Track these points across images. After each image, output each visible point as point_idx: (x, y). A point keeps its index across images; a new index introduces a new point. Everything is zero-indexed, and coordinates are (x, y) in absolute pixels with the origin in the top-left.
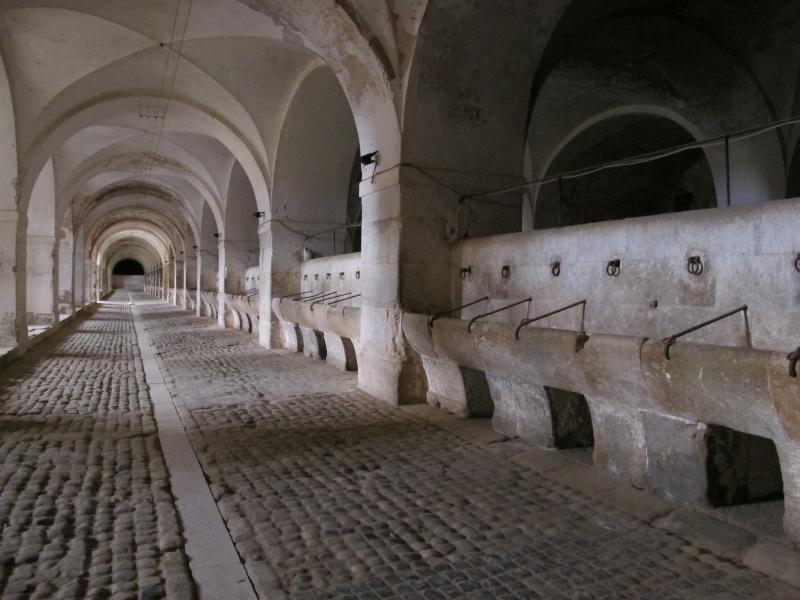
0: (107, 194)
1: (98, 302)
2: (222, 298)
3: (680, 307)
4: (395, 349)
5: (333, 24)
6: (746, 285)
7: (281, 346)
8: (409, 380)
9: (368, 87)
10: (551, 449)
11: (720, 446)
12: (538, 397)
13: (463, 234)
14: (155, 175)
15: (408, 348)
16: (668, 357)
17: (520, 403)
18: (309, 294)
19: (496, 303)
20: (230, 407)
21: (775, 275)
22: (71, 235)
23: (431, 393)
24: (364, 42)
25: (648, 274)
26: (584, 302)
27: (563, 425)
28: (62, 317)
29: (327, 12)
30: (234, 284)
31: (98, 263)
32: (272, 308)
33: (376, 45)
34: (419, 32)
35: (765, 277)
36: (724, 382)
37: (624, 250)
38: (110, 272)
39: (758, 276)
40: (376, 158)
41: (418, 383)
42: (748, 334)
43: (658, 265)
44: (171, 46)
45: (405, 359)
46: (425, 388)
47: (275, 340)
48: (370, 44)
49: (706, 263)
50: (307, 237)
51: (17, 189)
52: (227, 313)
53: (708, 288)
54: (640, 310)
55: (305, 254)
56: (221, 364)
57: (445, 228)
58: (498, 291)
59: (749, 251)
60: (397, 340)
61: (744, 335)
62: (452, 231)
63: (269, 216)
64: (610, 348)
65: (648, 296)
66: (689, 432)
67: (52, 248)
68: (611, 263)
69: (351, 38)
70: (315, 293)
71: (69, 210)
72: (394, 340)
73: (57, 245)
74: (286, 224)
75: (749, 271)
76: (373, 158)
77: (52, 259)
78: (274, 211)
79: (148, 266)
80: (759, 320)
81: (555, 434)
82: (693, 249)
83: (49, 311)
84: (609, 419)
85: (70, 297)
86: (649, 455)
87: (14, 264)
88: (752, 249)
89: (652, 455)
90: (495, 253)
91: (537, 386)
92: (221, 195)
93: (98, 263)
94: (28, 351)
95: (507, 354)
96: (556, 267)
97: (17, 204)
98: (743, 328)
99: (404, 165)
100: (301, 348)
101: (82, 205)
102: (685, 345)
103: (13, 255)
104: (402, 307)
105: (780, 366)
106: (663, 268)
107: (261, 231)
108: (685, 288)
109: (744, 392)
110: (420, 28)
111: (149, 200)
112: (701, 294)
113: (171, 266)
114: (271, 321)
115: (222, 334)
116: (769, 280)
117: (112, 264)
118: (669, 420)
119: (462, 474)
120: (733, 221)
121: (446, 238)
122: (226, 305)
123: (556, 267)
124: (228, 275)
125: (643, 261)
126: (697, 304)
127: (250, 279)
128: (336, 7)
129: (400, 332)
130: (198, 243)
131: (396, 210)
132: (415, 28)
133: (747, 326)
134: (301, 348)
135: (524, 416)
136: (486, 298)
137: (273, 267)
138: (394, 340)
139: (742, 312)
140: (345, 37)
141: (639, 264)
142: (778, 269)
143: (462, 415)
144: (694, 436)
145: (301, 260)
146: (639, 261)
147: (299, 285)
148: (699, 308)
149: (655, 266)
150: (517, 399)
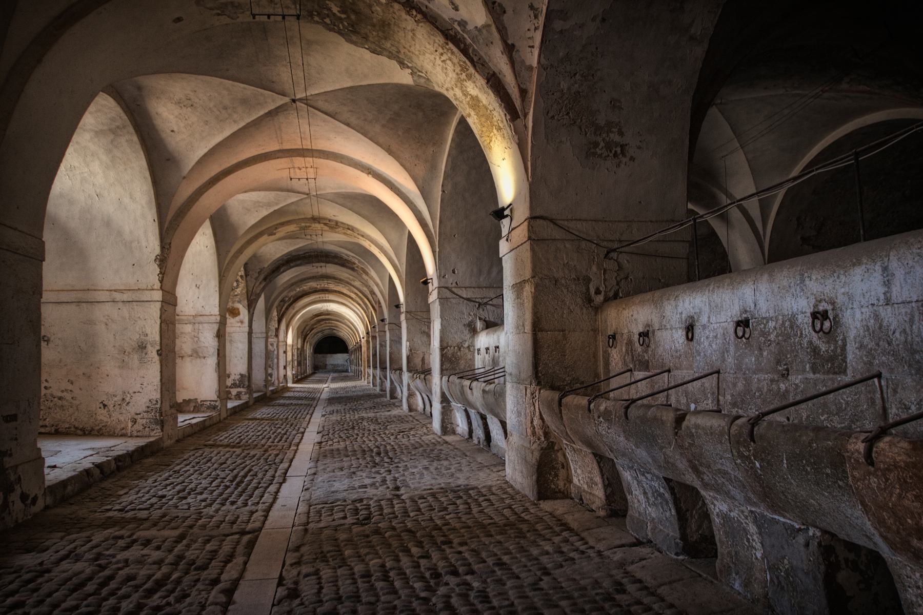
0: (283, 265)
1: (290, 385)
2: (406, 376)
3: (811, 376)
4: (534, 433)
5: (448, 62)
6: (878, 345)
7: (454, 432)
8: (547, 468)
9: (495, 131)
10: (681, 557)
11: (846, 560)
12: (662, 490)
13: (611, 294)
14: (330, 240)
15: (547, 434)
16: (753, 440)
17: (647, 498)
18: (482, 370)
19: (639, 375)
20: (354, 501)
21: (908, 330)
22: (246, 312)
23: (575, 486)
24: (481, 81)
25: (777, 336)
26: (718, 372)
27: (694, 527)
28: (230, 405)
29: (440, 50)
30: (418, 361)
31: (290, 340)
32: (441, 388)
33: (495, 83)
34: (539, 62)
35: (897, 334)
36: (807, 473)
37: (752, 306)
38: (309, 350)
39: (890, 333)
40: (511, 211)
41: (562, 473)
42: (885, 409)
43: (787, 324)
44: (305, 100)
45: (544, 445)
46: (569, 480)
47: (447, 427)
48: (487, 83)
49: (834, 318)
50: (480, 304)
51: (160, 266)
52: (411, 395)
53: (839, 350)
54: (772, 381)
55: (479, 325)
56: (379, 454)
57: (588, 289)
58: (640, 361)
59: (878, 300)
60: (535, 423)
61: (881, 411)
62: (598, 292)
63: (436, 284)
64: (703, 428)
65: (778, 362)
66: (801, 539)
67: (216, 327)
68: (738, 324)
69: (469, 77)
70: (487, 369)
71: (242, 285)
72: (532, 422)
73: (222, 323)
74: (454, 290)
75: (880, 327)
76: (506, 212)
77: (216, 339)
78: (441, 277)
79: (351, 345)
80: (895, 391)
81: (684, 537)
82: (820, 301)
83: (213, 396)
84: (725, 517)
85: (246, 380)
86: (769, 568)
87: (158, 348)
88: (882, 297)
89: (773, 568)
90: (634, 316)
91: (658, 478)
92: (399, 261)
93: (290, 340)
94: (178, 441)
95: (622, 439)
96: (690, 329)
97: (161, 282)
98: (879, 402)
99: (533, 218)
100: (471, 431)
101: (256, 279)
102: (770, 423)
103: (158, 338)
104: (539, 384)
105: (857, 451)
106: (792, 327)
107: (431, 300)
108: (815, 351)
109: (828, 486)
110: (539, 56)
111: (331, 269)
112: (832, 359)
113: (368, 342)
114: (442, 402)
115: (401, 419)
116: (903, 338)
117: (313, 339)
118: (778, 522)
119: (640, 581)
120: (859, 263)
121: (590, 300)
122: (409, 385)
123: (690, 329)
124: (411, 350)
125: (771, 319)
126: (828, 372)
127: (483, 351)
128: (447, 44)
129: (537, 414)
130: (386, 316)
131: (528, 274)
132: (533, 58)
133: (883, 398)
134: (471, 431)
135: (653, 515)
136: (630, 370)
137: (441, 341)
138: (532, 422)
139: (876, 380)
140: (464, 76)
141: (768, 322)
142: (912, 321)
143: (602, 513)
144: (807, 545)
145: (474, 332)
146: (768, 319)
147: (473, 360)
148: (831, 376)
149: (783, 323)
150: (645, 493)
